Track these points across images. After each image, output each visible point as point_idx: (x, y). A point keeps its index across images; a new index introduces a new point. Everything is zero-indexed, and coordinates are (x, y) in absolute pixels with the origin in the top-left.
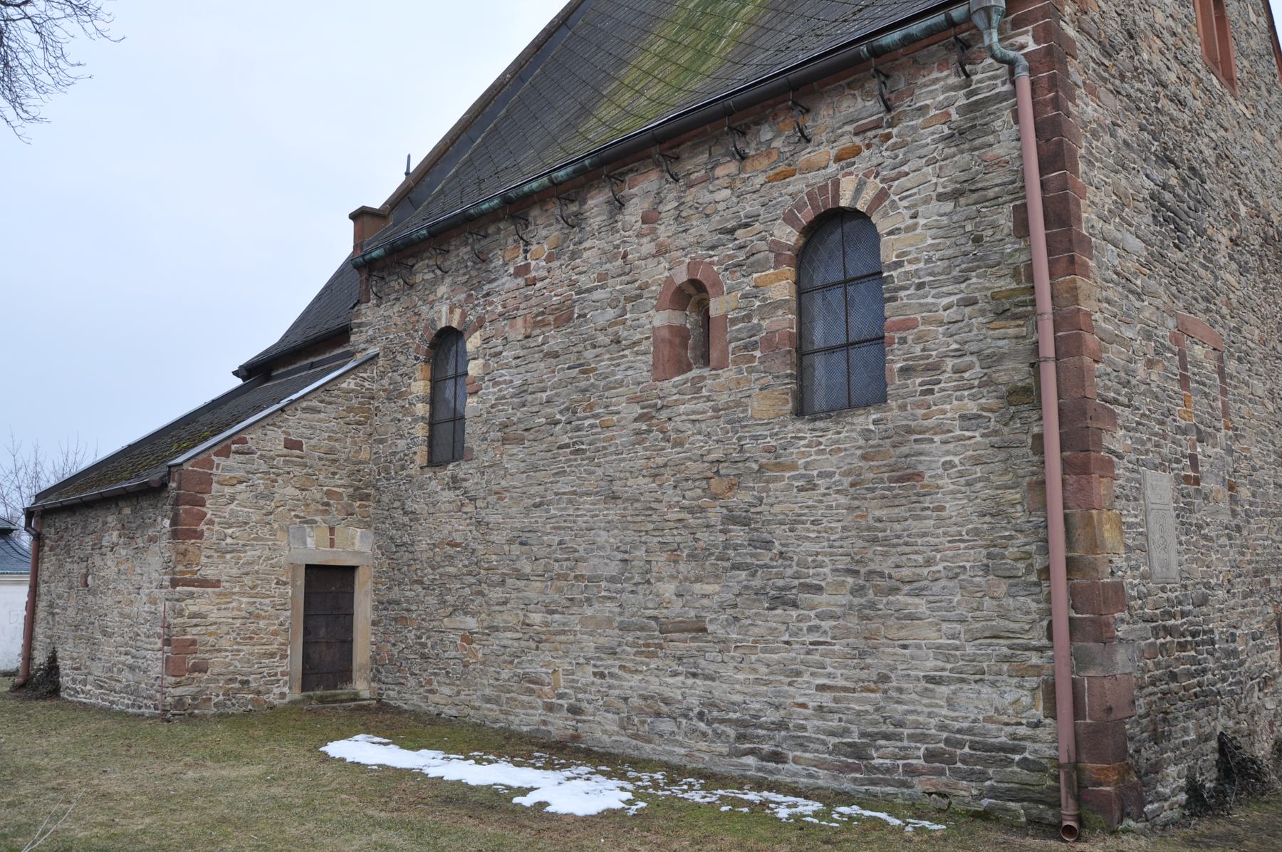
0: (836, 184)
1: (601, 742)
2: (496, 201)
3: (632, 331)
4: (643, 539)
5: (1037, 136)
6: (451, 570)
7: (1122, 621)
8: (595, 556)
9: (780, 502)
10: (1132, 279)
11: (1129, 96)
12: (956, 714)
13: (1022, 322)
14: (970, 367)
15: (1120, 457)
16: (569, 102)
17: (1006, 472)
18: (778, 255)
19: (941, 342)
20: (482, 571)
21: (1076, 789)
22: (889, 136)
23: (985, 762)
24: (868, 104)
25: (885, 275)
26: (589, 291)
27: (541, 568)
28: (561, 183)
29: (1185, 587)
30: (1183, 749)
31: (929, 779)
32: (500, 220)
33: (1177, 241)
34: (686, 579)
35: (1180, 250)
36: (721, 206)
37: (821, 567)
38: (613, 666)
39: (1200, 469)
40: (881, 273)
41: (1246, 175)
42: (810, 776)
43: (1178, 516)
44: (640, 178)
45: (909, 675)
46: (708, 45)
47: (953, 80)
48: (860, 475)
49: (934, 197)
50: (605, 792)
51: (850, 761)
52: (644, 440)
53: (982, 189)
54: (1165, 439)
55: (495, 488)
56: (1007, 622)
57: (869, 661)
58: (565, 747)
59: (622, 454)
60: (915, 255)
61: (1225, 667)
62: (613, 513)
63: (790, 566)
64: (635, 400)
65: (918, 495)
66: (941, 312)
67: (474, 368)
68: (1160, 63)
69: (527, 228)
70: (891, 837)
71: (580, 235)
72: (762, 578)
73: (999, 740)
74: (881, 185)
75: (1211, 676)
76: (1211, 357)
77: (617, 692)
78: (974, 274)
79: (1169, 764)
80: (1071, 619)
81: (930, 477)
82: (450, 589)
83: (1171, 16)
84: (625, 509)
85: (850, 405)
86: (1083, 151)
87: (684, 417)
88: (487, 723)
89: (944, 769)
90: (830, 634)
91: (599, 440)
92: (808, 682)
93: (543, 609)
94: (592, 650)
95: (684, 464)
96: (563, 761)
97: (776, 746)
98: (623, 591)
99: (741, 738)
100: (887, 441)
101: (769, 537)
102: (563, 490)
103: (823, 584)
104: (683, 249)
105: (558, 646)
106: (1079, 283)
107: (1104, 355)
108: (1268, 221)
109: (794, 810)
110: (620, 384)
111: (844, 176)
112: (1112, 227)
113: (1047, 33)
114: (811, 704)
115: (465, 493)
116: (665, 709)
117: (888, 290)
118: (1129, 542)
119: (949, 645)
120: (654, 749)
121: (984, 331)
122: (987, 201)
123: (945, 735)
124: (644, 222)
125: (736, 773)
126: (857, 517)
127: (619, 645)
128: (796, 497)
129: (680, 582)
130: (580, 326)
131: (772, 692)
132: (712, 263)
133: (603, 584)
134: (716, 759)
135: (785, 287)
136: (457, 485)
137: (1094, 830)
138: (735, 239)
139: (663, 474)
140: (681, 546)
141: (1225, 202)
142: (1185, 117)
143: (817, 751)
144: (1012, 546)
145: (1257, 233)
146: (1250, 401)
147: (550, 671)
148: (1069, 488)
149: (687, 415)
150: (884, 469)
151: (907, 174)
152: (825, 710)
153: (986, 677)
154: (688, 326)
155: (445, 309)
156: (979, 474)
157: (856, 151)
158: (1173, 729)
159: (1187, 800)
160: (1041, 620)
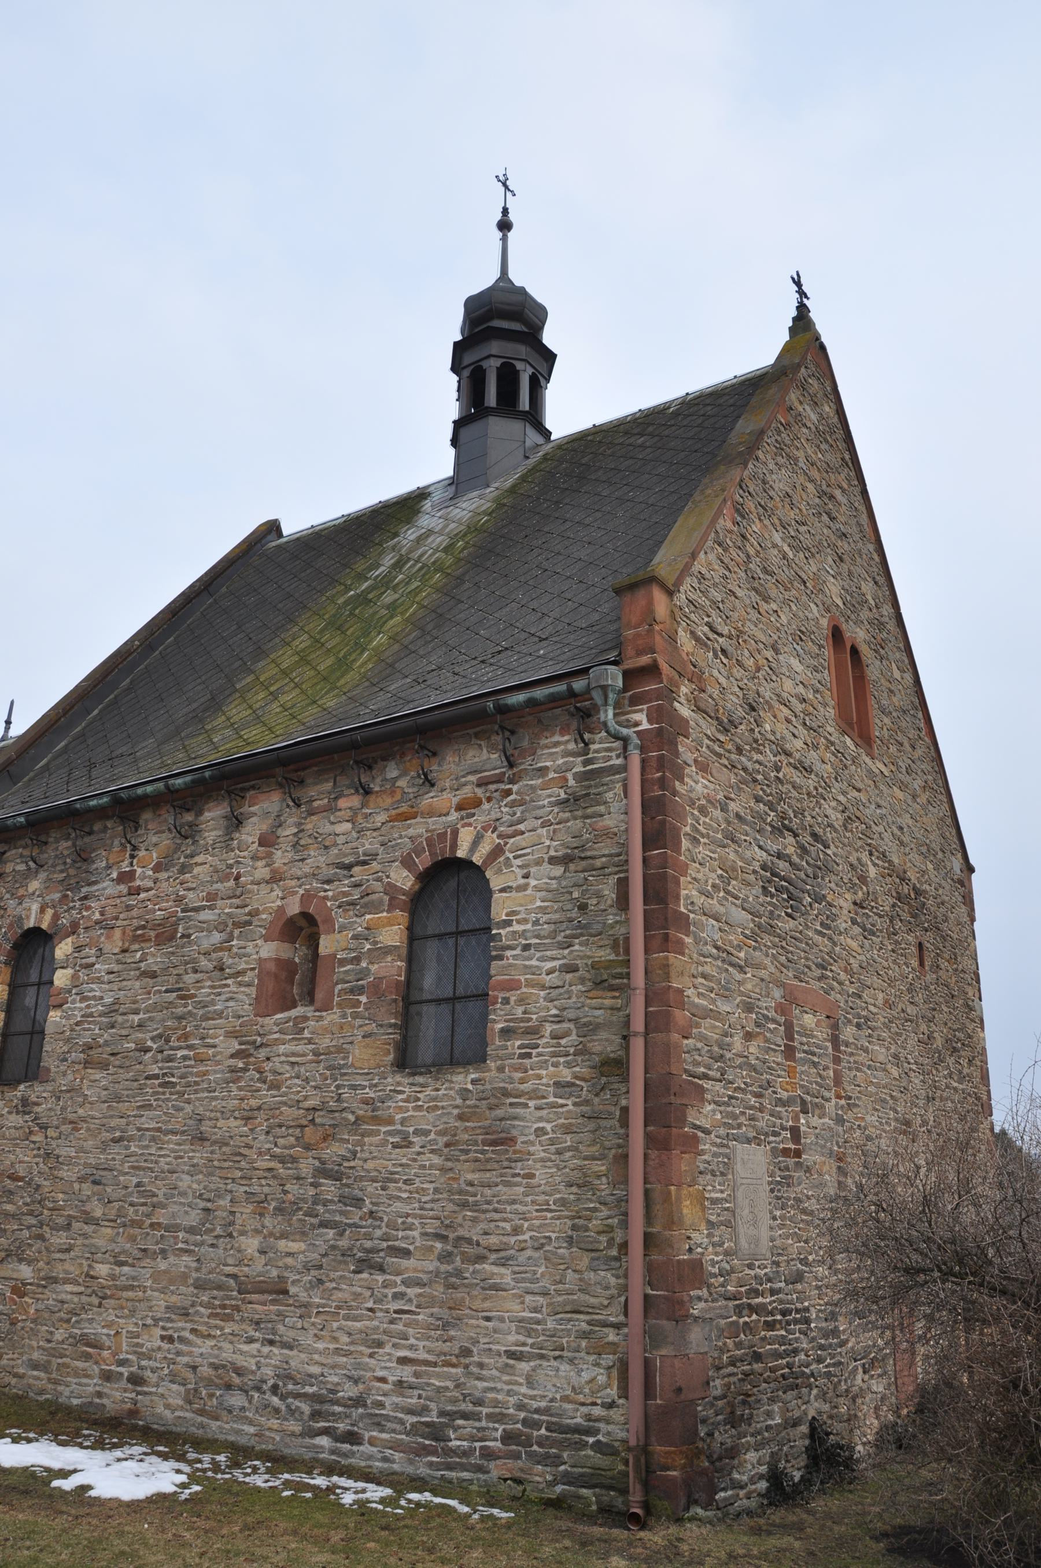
0: (455, 833)
1: (162, 1419)
2: (105, 799)
3: (237, 959)
4: (229, 1187)
5: (643, 813)
6: (9, 1207)
7: (699, 1299)
8: (175, 1203)
9: (374, 1158)
10: (734, 952)
11: (745, 769)
12: (535, 1392)
13: (617, 994)
14: (567, 1034)
15: (707, 1132)
16: (199, 688)
17: (594, 1143)
18: (392, 899)
19: (541, 1006)
20: (45, 1212)
21: (644, 1475)
22: (509, 792)
23: (561, 1445)
24: (493, 756)
25: (494, 932)
26: (196, 910)
27: (114, 1212)
28: (177, 791)
29: (777, 1264)
30: (766, 1434)
31: (505, 1464)
32: (108, 818)
33: (789, 911)
34: (271, 1234)
35: (793, 919)
36: (341, 840)
37: (411, 1229)
38: (183, 1329)
39: (803, 1141)
40: (489, 929)
41: (880, 834)
42: (385, 1459)
43: (772, 1191)
44: (262, 797)
45: (490, 1349)
46: (350, 654)
47: (572, 746)
48: (455, 1135)
49: (546, 860)
50: (158, 1475)
51: (427, 1442)
52: (238, 1079)
53: (590, 858)
54: (762, 1112)
55: (71, 1116)
56: (587, 1297)
57: (452, 1333)
58: (121, 1424)
59: (214, 1091)
60: (524, 916)
61: (822, 1347)
62: (199, 1156)
63: (380, 1227)
64: (232, 1034)
65: (510, 1160)
66: (544, 976)
67: (61, 978)
68: (785, 732)
69: (136, 831)
70: (454, 1524)
71: (193, 848)
72: (350, 1238)
73: (575, 1421)
74: (498, 841)
75: (803, 1357)
76: (824, 1024)
77: (185, 1360)
78: (577, 941)
79: (747, 1450)
80: (646, 1297)
81: (522, 1143)
82: (5, 1230)
83: (801, 682)
84: (212, 1152)
85: (451, 1061)
86: (688, 829)
87: (283, 1058)
88: (31, 1394)
89: (520, 1452)
90: (415, 1302)
91: (191, 1073)
92: (389, 1354)
93: (112, 1260)
94: (163, 1309)
95: (279, 1108)
96: (115, 1440)
97: (352, 1425)
98: (201, 1244)
99: (316, 1415)
100: (484, 1102)
101: (360, 1194)
102: (147, 1126)
103: (411, 1248)
104: (298, 879)
105: (124, 1304)
106: (671, 961)
107: (694, 1030)
108: (902, 879)
109: (360, 1496)
110: (220, 1015)
111: (463, 826)
112: (715, 902)
113: (662, 714)
114: (391, 1379)
115: (36, 1119)
116: (236, 1380)
117: (496, 948)
118: (713, 1218)
119: (531, 1318)
120: (220, 1427)
121: (582, 999)
122: (595, 870)
123: (522, 1415)
124: (260, 845)
125: (308, 1456)
126: (449, 1179)
127: (193, 1306)
128: (390, 1153)
129: (265, 1238)
130: (183, 947)
131: (351, 1364)
132: (326, 898)
133: (181, 1235)
134: (287, 1440)
135: (396, 933)
136: (27, 1109)
137: (660, 1517)
138: (352, 876)
139: (256, 1118)
140: (269, 1198)
141: (851, 865)
142: (811, 783)
143: (394, 1431)
144: (596, 1219)
145: (888, 893)
146: (869, 1067)
147: (112, 1333)
148: (651, 1163)
149: (287, 1056)
150: (479, 1131)
151: (523, 833)
152: (405, 1385)
153: (565, 1354)
154: (297, 960)
155: (35, 907)
156: (569, 1143)
157: (477, 803)
158: (755, 1412)
159: (768, 1489)
160: (620, 1296)
